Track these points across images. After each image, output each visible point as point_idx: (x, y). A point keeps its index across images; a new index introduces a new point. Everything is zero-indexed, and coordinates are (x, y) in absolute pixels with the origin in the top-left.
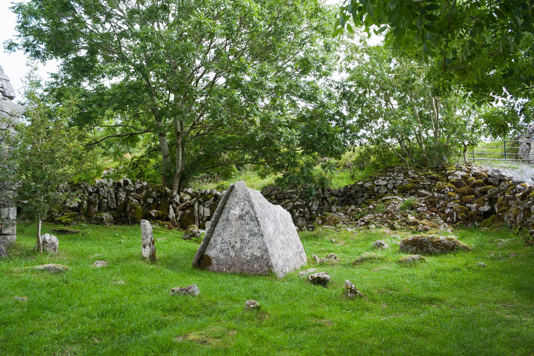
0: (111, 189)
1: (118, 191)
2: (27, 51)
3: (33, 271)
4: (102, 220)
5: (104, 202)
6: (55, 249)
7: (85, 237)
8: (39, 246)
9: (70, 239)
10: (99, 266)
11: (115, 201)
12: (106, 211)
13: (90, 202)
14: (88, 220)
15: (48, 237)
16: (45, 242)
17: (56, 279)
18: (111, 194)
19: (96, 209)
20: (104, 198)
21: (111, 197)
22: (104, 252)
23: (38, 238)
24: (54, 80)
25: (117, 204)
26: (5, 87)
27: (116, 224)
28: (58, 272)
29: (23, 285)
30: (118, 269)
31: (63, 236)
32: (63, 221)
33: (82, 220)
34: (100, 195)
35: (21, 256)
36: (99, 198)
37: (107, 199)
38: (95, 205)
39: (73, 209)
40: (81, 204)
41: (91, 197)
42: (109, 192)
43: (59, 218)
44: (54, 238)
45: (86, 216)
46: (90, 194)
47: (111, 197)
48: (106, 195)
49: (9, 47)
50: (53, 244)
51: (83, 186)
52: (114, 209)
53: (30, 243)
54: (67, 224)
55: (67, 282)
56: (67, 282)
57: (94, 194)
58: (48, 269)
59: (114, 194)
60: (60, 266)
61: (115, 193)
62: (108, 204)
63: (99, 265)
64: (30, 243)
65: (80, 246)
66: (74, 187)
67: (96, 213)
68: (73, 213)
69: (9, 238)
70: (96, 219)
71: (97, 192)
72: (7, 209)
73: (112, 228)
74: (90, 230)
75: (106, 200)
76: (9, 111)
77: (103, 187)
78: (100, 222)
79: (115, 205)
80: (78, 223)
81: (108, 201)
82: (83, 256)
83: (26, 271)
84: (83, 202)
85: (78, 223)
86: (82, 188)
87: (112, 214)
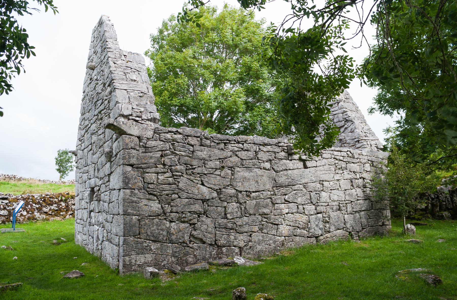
0: (448, 195)
1: (453, 196)
2: (381, 111)
3: (405, 242)
4: (442, 216)
5: (443, 205)
6: (414, 233)
7: (430, 227)
8: (405, 231)
9: (421, 228)
10: (440, 241)
11: (451, 203)
12: (445, 211)
13: (433, 205)
14: (433, 217)
15: (409, 226)
16: (408, 228)
17: (417, 246)
18: (448, 199)
19: (438, 209)
20: (443, 201)
21: (448, 201)
22: (445, 235)
23: (404, 227)
24: (398, 125)
25: (453, 206)
26: (378, 144)
27: (453, 219)
28: (417, 243)
29: (402, 247)
30: (452, 243)
31: (418, 227)
32: (416, 218)
33: (428, 217)
34: (440, 199)
35: (395, 236)
36: (439, 201)
37: (445, 202)
38: (437, 206)
39: (422, 210)
40: (427, 207)
41: (433, 201)
42: (446, 197)
43: (413, 216)
44: (413, 227)
45: (431, 214)
46: (433, 199)
47: (448, 201)
48: (444, 199)
49: (371, 111)
50: (412, 230)
51: (427, 194)
52: (451, 209)
53: (400, 230)
54: (419, 219)
55: (423, 248)
56: (423, 248)
57: (435, 199)
58: (412, 241)
59: (450, 199)
60: (418, 240)
61: (451, 197)
62: (446, 206)
63: (441, 241)
64: (400, 230)
65: (428, 232)
66: (422, 196)
67: (438, 212)
68: (421, 212)
69: (388, 227)
70: (438, 216)
71: (438, 197)
72: (385, 211)
73: (450, 221)
74: (435, 223)
75: (444, 203)
76: (381, 157)
77: (441, 194)
78: (441, 218)
79: (452, 206)
80: (426, 219)
81: (446, 204)
82: (431, 237)
83: (401, 242)
84: (428, 205)
85: (426, 219)
86: (426, 196)
87: (450, 212)
